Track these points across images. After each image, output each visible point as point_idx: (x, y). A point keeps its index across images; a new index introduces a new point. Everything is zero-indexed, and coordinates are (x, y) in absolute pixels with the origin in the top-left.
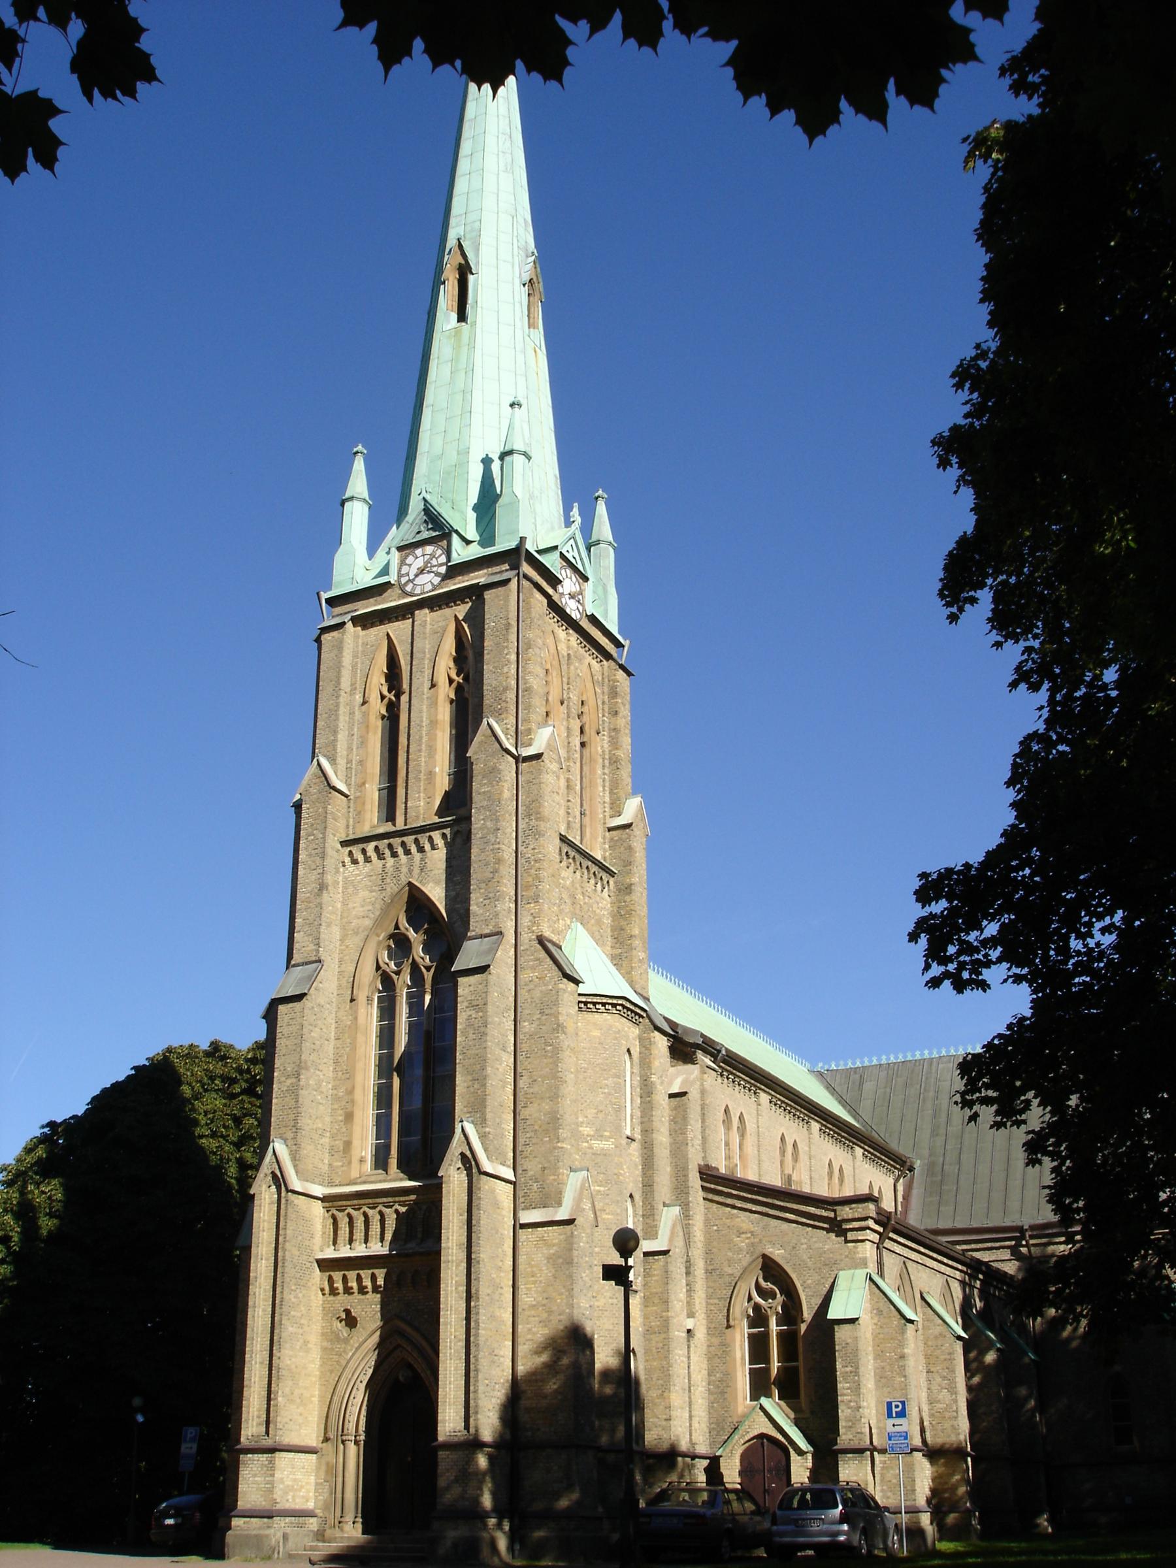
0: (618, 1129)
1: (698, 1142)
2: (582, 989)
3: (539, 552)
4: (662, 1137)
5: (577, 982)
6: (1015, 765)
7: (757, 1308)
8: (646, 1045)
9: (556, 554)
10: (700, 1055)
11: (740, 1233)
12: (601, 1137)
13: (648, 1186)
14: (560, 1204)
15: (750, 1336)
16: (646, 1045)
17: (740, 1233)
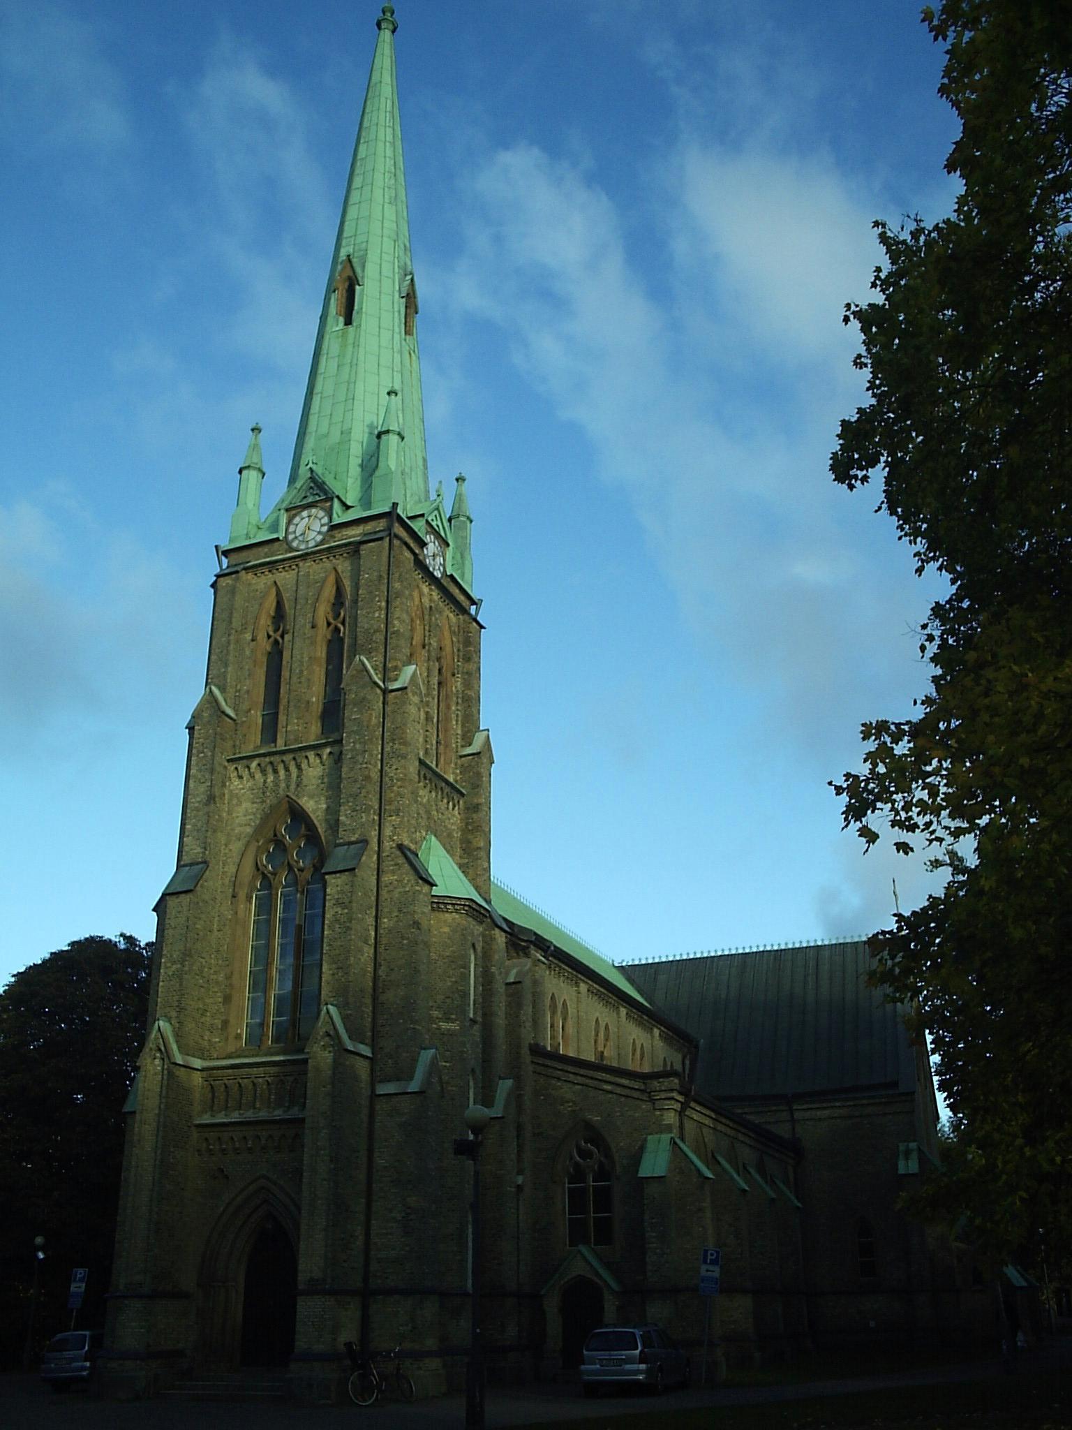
0: (464, 1012)
2: (435, 891)
3: (409, 518)
5: (432, 885)
12: (448, 1020)
14: (411, 1078)
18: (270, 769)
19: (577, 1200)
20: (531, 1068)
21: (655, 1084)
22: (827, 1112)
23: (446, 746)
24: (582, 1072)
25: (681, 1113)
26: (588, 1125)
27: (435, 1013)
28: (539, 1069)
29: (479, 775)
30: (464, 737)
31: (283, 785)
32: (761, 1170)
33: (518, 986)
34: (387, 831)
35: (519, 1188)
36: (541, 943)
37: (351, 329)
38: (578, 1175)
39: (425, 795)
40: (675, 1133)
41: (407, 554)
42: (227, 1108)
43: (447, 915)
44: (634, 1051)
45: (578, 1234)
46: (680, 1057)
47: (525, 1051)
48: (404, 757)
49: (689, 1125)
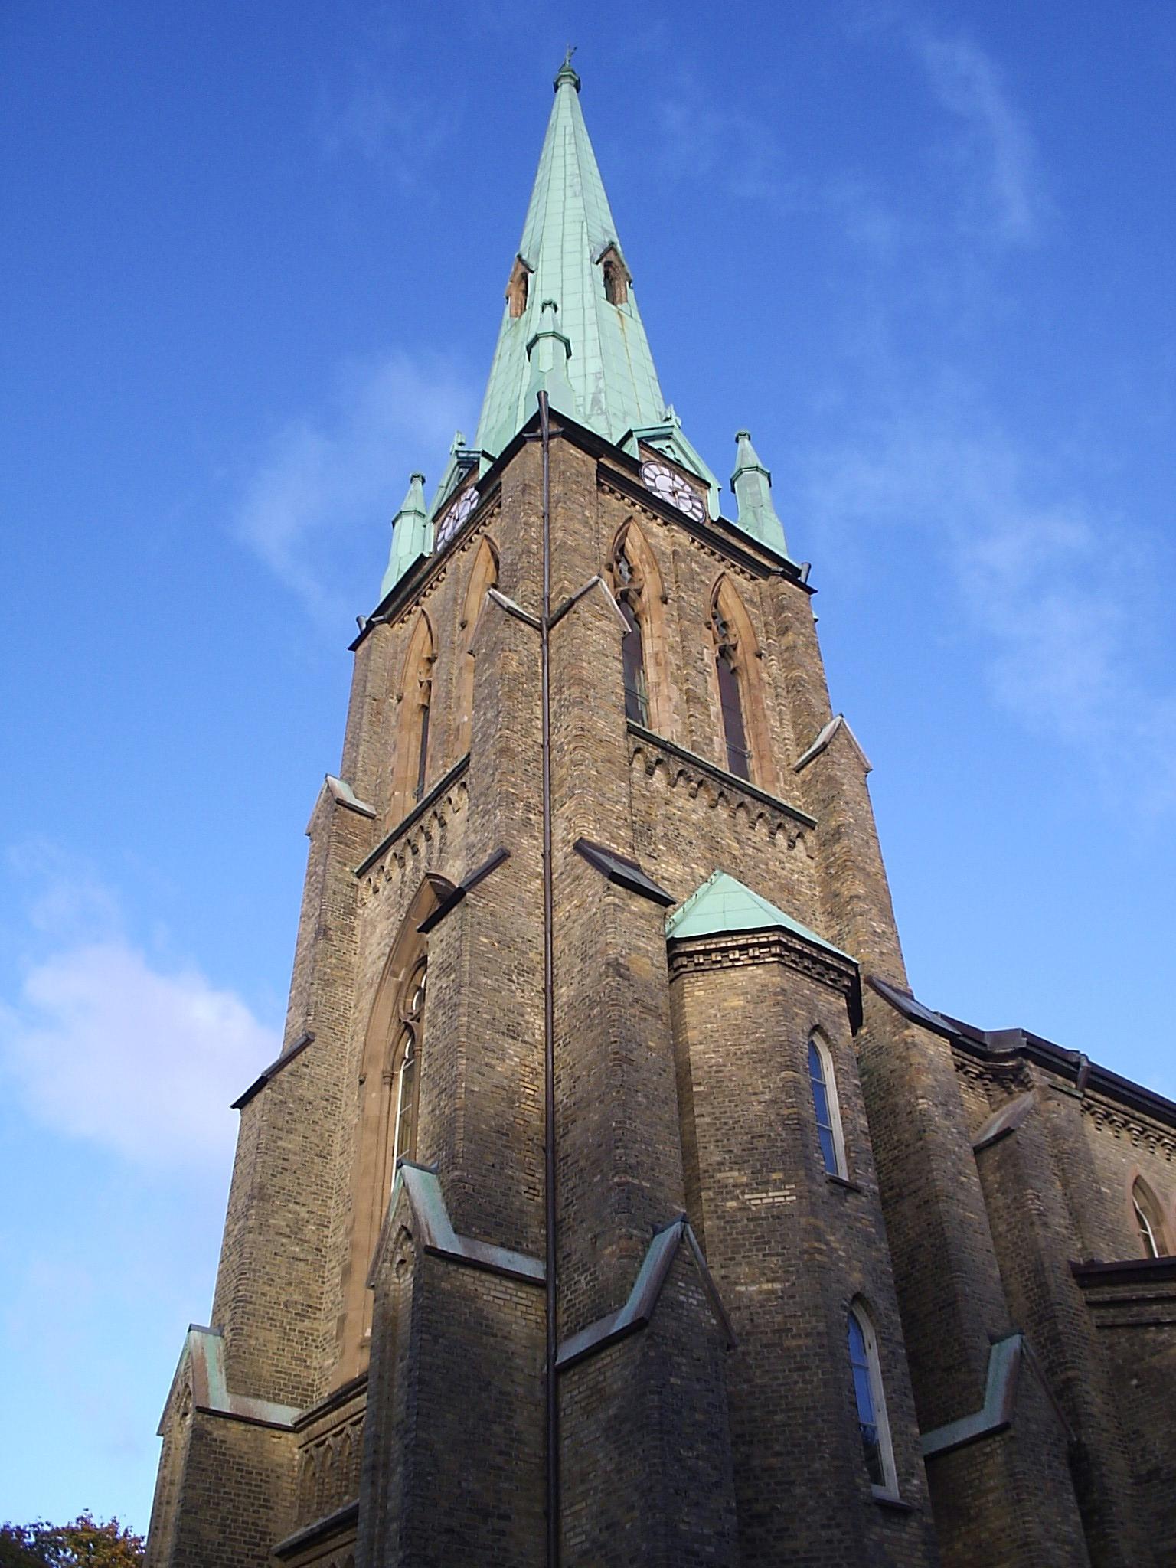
12: (764, 1185)
20: (1089, 1320)
23: (761, 758)
24: (402, 595)
27: (734, 1176)
28: (1109, 1315)
33: (1009, 1141)
42: (182, 1530)
43: (734, 974)
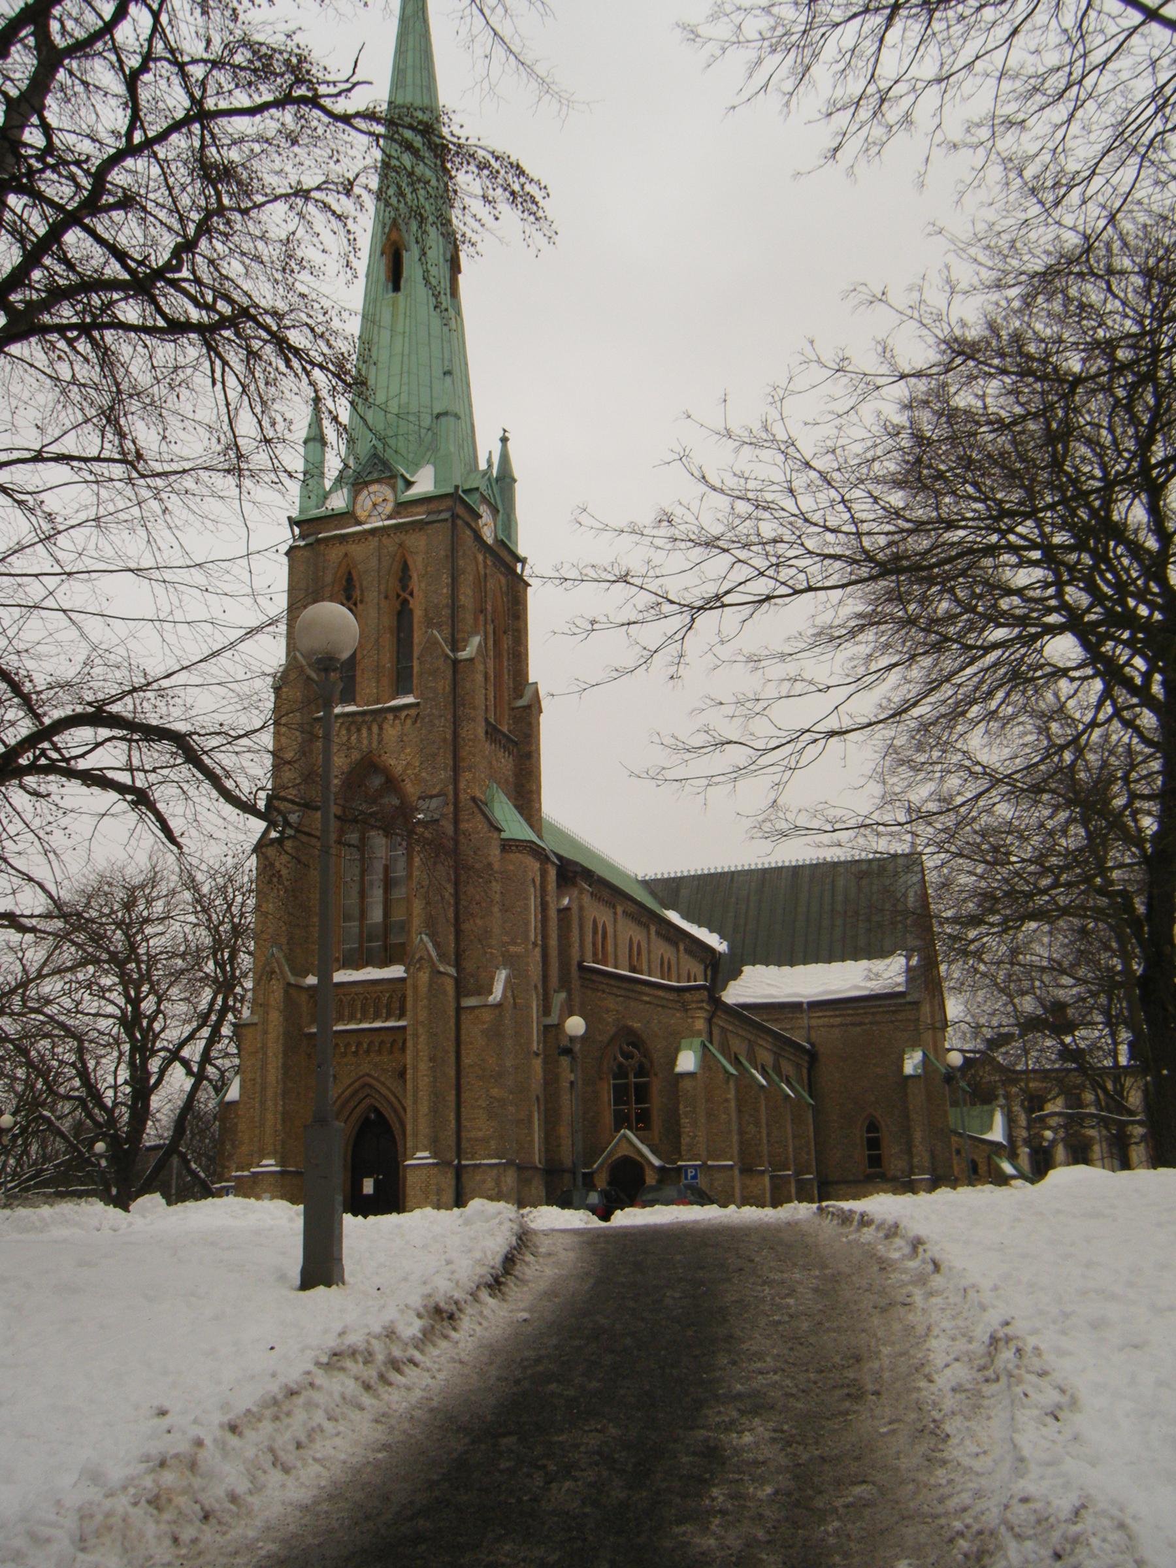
0: (527, 937)
1: (577, 945)
2: (504, 835)
3: (464, 491)
4: (553, 942)
5: (500, 830)
6: (933, 1186)
7: (620, 1065)
8: (544, 874)
9: (477, 496)
10: (578, 880)
11: (608, 1011)
12: (515, 944)
13: (545, 977)
14: (491, 993)
15: (615, 1086)
16: (544, 874)
17: (608, 1011)
18: (353, 729)
19: (620, 1094)
21: (687, 996)
22: (838, 1020)
24: (624, 985)
25: (710, 1021)
26: (630, 1031)
29: (530, 724)
30: (515, 689)
31: (365, 742)
32: (777, 1069)
34: (462, 785)
35: (572, 1083)
36: (588, 875)
37: (400, 296)
38: (621, 1073)
39: (488, 747)
40: (704, 1038)
41: (468, 532)
44: (662, 963)
45: (621, 1120)
46: (702, 967)
47: (574, 969)
48: (473, 720)
49: (716, 1031)
